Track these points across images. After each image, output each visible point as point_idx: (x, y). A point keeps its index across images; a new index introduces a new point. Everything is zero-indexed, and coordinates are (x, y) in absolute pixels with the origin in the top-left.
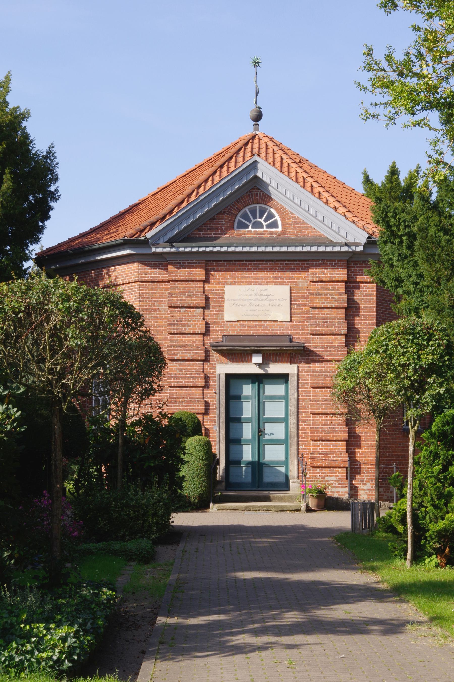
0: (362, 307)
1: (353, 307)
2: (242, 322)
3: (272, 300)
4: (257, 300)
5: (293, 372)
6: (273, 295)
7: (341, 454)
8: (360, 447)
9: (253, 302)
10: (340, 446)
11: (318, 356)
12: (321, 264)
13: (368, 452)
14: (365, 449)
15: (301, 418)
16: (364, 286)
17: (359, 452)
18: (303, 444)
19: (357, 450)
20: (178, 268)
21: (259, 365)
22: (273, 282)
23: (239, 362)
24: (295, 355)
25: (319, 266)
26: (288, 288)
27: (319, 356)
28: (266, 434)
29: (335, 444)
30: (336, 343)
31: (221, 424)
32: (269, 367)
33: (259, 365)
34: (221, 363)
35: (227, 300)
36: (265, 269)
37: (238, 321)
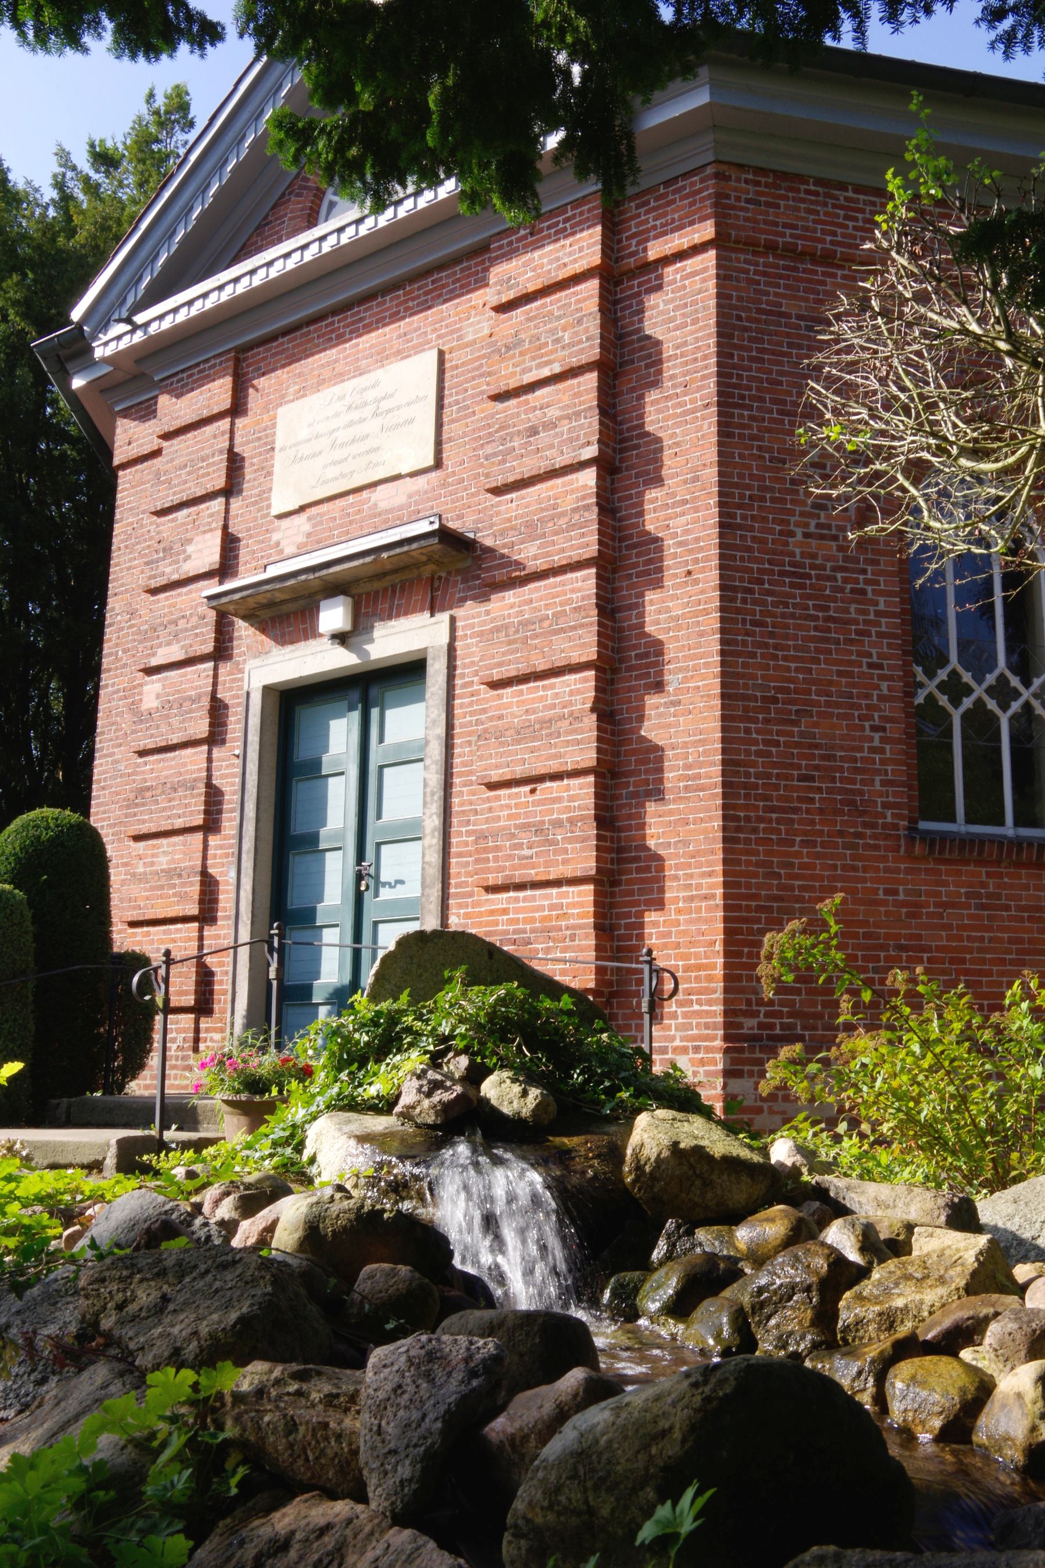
0: (668, 350)
1: (641, 359)
2: (313, 511)
3: (388, 411)
4: (351, 424)
5: (437, 643)
6: (392, 396)
7: (573, 938)
8: (659, 904)
9: (342, 436)
10: (574, 905)
11: (507, 562)
12: (525, 237)
13: (690, 922)
14: (679, 911)
15: (456, 809)
16: (677, 271)
17: (656, 924)
18: (460, 906)
19: (650, 917)
20: (178, 397)
21: (341, 638)
22: (399, 352)
23: (298, 641)
24: (447, 580)
25: (517, 249)
26: (432, 356)
27: (510, 563)
28: (384, 884)
29: (560, 896)
30: (568, 503)
31: (244, 856)
32: (372, 641)
33: (341, 638)
34: (259, 654)
35: (282, 449)
36: (377, 322)
37: (302, 509)
